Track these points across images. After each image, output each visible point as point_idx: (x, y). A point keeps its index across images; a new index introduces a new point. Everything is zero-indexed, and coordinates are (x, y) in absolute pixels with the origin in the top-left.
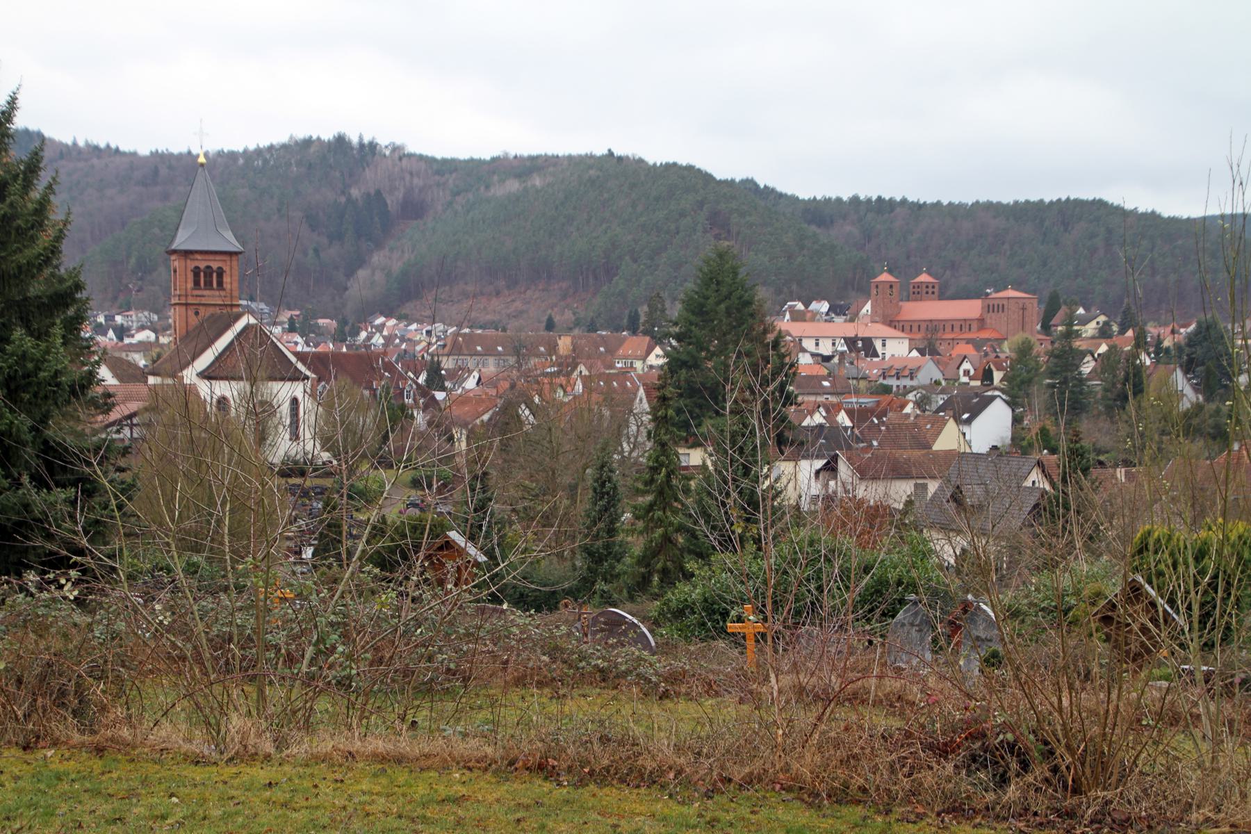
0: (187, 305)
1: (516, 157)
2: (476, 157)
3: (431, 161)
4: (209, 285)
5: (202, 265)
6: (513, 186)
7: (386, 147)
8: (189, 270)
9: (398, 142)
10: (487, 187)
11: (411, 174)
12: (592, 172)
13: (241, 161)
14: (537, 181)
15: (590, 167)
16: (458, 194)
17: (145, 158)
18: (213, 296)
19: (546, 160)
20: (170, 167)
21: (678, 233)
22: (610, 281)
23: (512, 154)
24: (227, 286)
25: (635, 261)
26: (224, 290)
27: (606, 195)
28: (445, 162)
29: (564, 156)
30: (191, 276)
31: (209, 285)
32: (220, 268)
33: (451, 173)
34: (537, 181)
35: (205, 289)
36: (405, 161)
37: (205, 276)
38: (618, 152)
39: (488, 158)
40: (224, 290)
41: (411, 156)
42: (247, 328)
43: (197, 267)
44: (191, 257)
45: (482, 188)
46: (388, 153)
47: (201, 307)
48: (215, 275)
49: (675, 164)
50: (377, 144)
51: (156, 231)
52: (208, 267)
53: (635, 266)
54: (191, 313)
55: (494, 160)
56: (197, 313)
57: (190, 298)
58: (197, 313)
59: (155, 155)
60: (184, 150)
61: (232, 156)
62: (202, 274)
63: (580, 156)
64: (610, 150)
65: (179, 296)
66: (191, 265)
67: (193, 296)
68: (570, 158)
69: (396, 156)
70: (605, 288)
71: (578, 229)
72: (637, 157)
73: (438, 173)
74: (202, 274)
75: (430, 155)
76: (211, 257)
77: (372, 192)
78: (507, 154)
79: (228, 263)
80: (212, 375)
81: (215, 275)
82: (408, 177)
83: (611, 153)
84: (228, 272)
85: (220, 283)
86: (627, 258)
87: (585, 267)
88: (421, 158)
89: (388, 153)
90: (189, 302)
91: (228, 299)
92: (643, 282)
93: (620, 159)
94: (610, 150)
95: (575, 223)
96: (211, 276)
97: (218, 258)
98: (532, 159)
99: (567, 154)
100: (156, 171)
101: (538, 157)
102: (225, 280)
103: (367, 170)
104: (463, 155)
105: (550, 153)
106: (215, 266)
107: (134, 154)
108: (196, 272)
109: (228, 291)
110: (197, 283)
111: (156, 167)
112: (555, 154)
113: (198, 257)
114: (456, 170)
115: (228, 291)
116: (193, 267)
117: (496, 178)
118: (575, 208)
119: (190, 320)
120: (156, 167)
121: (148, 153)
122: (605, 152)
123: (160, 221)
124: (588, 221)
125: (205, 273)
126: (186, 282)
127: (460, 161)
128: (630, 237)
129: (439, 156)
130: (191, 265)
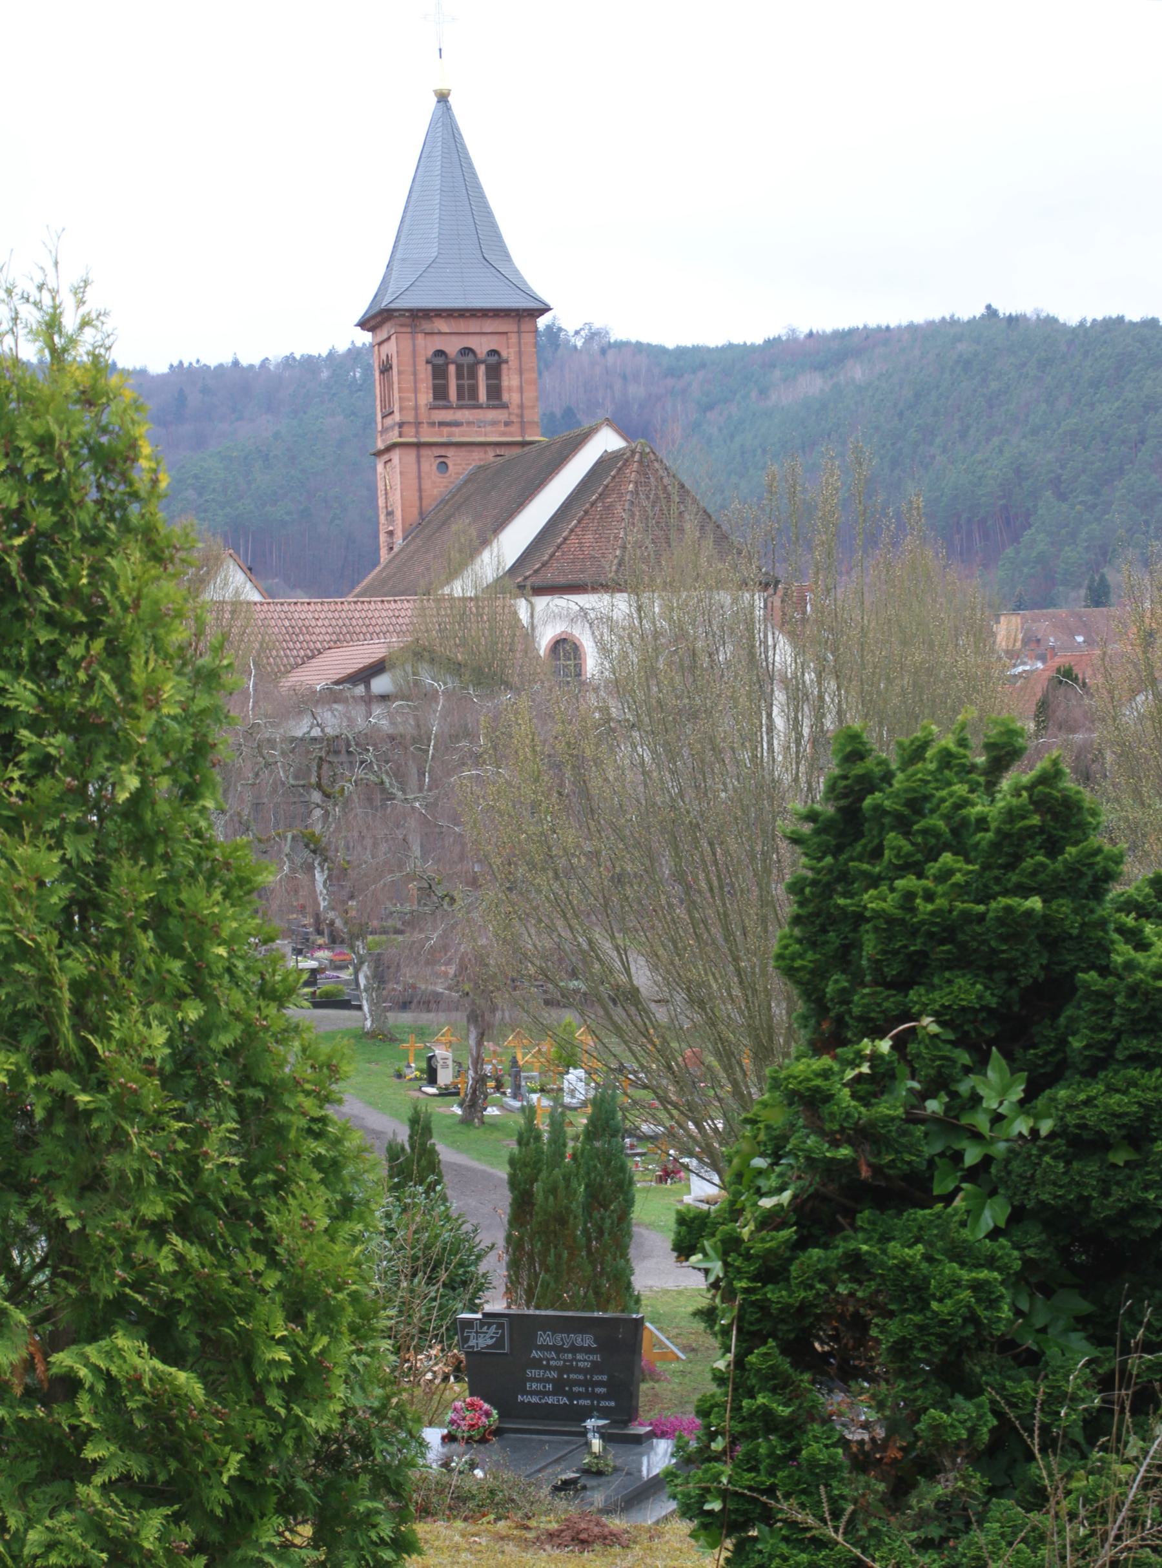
0: (418, 445)
1: (811, 335)
2: (737, 340)
3: (657, 352)
4: (468, 395)
5: (452, 346)
6: (812, 385)
7: (577, 333)
8: (421, 360)
9: (598, 325)
10: (763, 392)
11: (624, 377)
12: (961, 347)
13: (325, 374)
14: (857, 372)
15: (958, 339)
16: (710, 407)
17: (162, 378)
18: (480, 424)
19: (867, 338)
20: (205, 391)
21: (1142, 442)
22: (1016, 539)
23: (803, 331)
24: (511, 396)
25: (1062, 497)
26: (505, 406)
27: (994, 385)
28: (681, 352)
29: (899, 327)
30: (425, 372)
31: (468, 395)
32: (493, 352)
33: (694, 373)
34: (857, 372)
35: (460, 407)
36: (611, 356)
37: (459, 376)
38: (1005, 308)
39: (759, 341)
40: (505, 406)
41: (621, 346)
42: (605, 463)
43: (440, 353)
44: (427, 326)
45: (754, 394)
46: (579, 344)
47: (451, 452)
48: (482, 369)
49: (1120, 319)
50: (560, 329)
51: (190, 494)
52: (467, 351)
53: (1064, 507)
54: (429, 465)
55: (769, 343)
56: (443, 466)
57: (425, 428)
58: (443, 466)
59: (178, 370)
60: (227, 360)
61: (310, 364)
62: (452, 369)
63: (931, 324)
64: (989, 307)
65: (401, 425)
66: (427, 346)
67: (432, 424)
68: (912, 328)
69: (595, 347)
70: (1010, 551)
71: (944, 451)
72: (1043, 315)
73: (671, 372)
74: (452, 369)
75: (654, 341)
76: (473, 325)
77: (558, 413)
78: (793, 331)
79: (513, 338)
80: (549, 576)
81: (482, 369)
82: (618, 385)
83: (991, 312)
84: (513, 363)
85: (495, 392)
86: (1049, 493)
87: (964, 516)
88: (639, 347)
89: (579, 344)
90: (423, 440)
91: (514, 428)
92: (1083, 535)
93: (1012, 320)
94: (989, 307)
95: (938, 440)
96: (473, 375)
97: (490, 326)
98: (841, 336)
99: (904, 323)
100: (181, 398)
101: (852, 332)
102: (505, 382)
103: (546, 374)
104: (713, 338)
105: (872, 324)
106: (482, 346)
107: (142, 373)
108: (439, 364)
109: (514, 409)
110: (440, 393)
111: (181, 390)
112: (884, 324)
113: (442, 325)
114: (703, 366)
115: (514, 409)
116: (430, 353)
117: (777, 373)
118: (936, 413)
119: (427, 484)
120: (181, 390)
121: (165, 370)
122: (979, 311)
123: (196, 477)
124: (963, 435)
125: (459, 368)
126: (416, 391)
127: (708, 350)
128: (1050, 456)
129: (670, 345)
130: (427, 346)
